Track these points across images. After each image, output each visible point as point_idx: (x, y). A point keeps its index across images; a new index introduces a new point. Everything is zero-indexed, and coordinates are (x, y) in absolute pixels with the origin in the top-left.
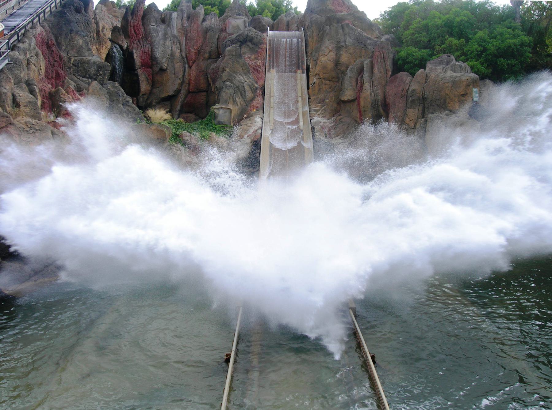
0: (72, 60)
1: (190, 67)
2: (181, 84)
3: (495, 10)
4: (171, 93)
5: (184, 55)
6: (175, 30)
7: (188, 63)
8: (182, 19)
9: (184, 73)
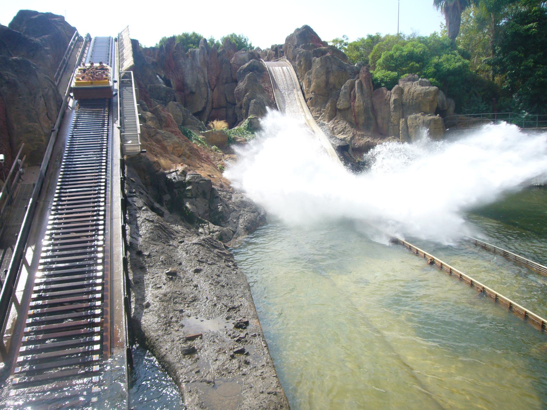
0: (148, 87)
1: (213, 90)
2: (206, 103)
3: (392, 37)
4: (200, 109)
5: (207, 81)
6: (199, 63)
7: (210, 87)
8: (204, 55)
9: (208, 94)
